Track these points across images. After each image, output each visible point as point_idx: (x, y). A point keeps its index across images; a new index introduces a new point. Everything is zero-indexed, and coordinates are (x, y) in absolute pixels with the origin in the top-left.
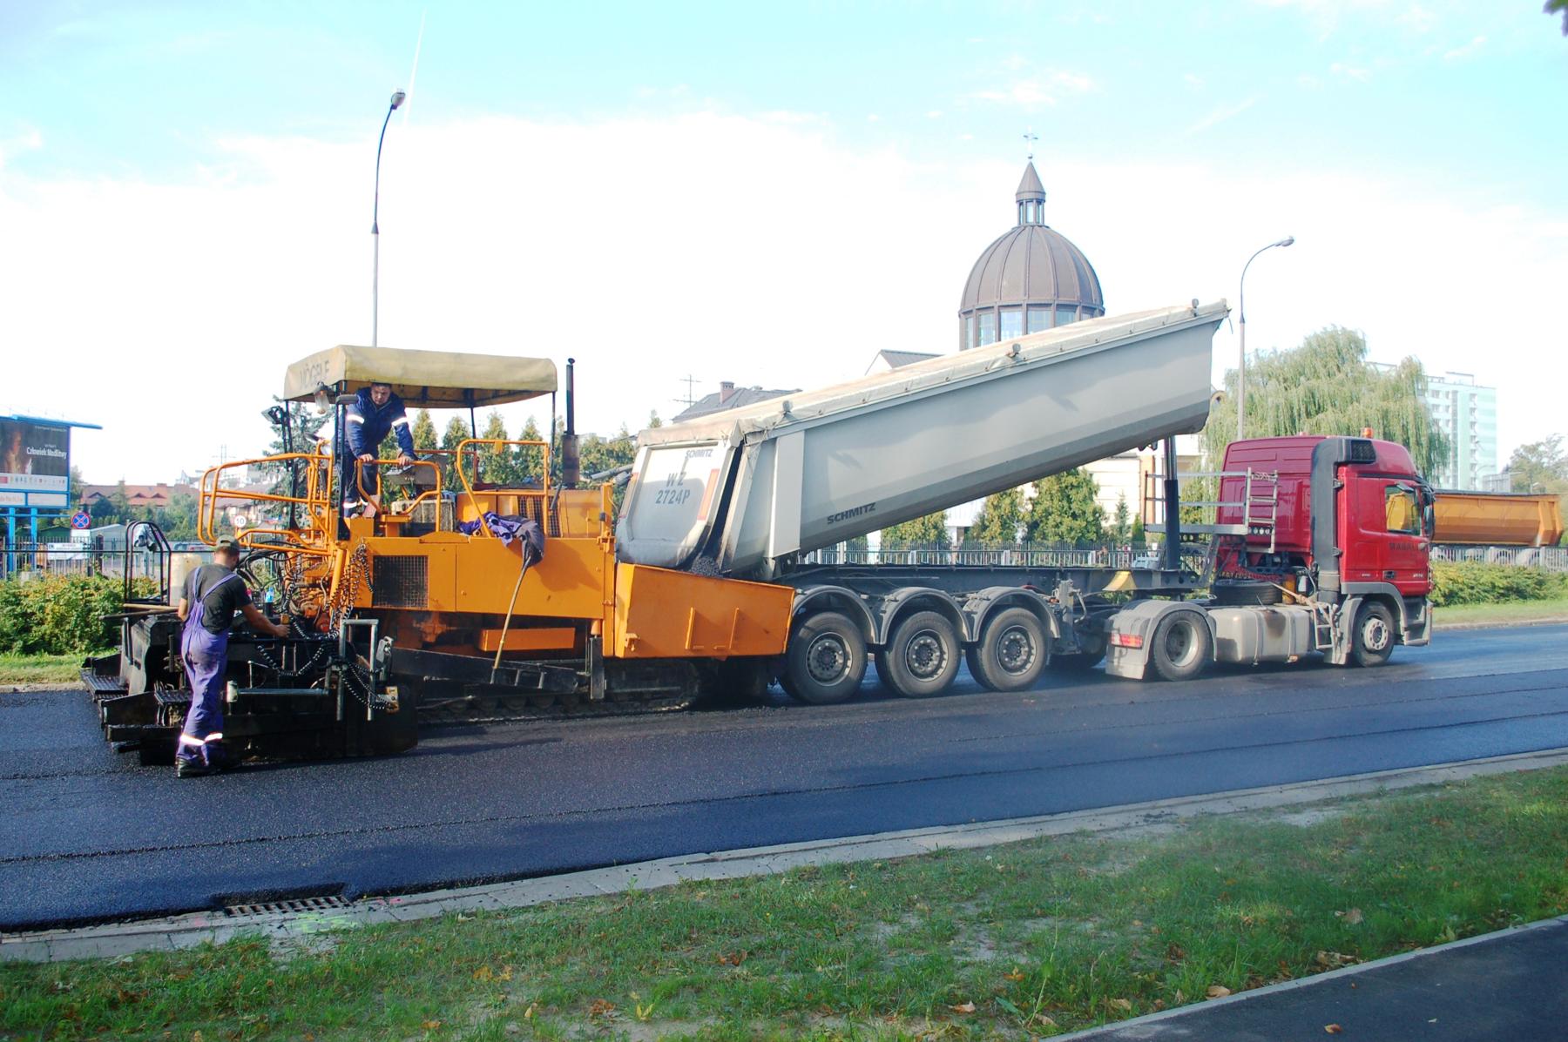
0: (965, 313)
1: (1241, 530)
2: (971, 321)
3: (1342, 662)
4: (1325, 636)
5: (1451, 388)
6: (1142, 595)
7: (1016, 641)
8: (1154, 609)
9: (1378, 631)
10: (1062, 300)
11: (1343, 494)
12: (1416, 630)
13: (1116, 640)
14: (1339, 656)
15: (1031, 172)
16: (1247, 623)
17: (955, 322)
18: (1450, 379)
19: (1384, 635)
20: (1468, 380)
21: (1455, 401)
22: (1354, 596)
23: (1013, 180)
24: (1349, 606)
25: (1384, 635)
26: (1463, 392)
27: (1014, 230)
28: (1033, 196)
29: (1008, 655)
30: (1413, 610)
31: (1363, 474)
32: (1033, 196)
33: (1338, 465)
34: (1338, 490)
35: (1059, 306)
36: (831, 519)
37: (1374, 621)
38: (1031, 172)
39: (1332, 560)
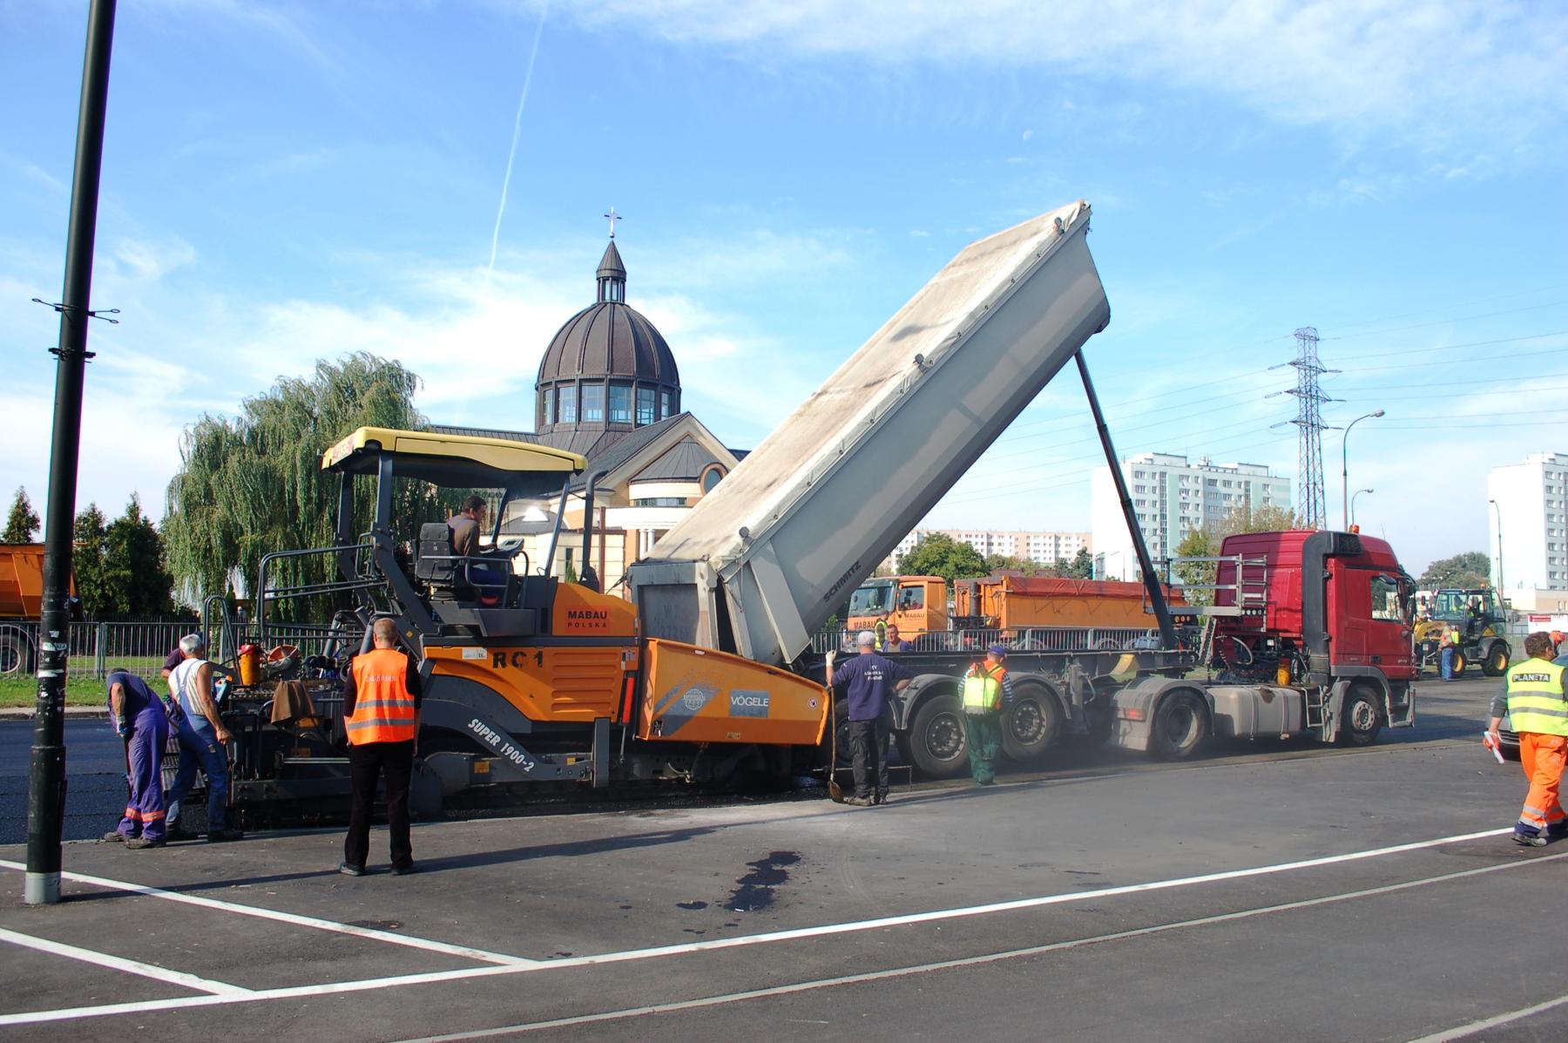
0: (541, 387)
1: (1234, 611)
2: (550, 394)
3: (1332, 740)
4: (1315, 717)
5: (1243, 479)
6: (1143, 675)
7: (1028, 714)
8: (1157, 684)
9: (1364, 712)
10: (617, 375)
11: (1332, 584)
12: (1400, 712)
13: (1121, 715)
14: (1330, 733)
15: (613, 252)
16: (1242, 699)
17: (531, 398)
18: (1242, 470)
19: (1371, 716)
20: (1262, 472)
21: (1162, 482)
22: (1342, 679)
23: (596, 256)
24: (1338, 687)
25: (1371, 716)
26: (1172, 473)
27: (594, 307)
28: (614, 274)
29: (1021, 726)
30: (1396, 696)
31: (1348, 565)
32: (614, 274)
33: (1327, 556)
34: (1326, 579)
35: (612, 382)
36: (827, 597)
37: (1361, 704)
38: (613, 252)
39: (1321, 646)
